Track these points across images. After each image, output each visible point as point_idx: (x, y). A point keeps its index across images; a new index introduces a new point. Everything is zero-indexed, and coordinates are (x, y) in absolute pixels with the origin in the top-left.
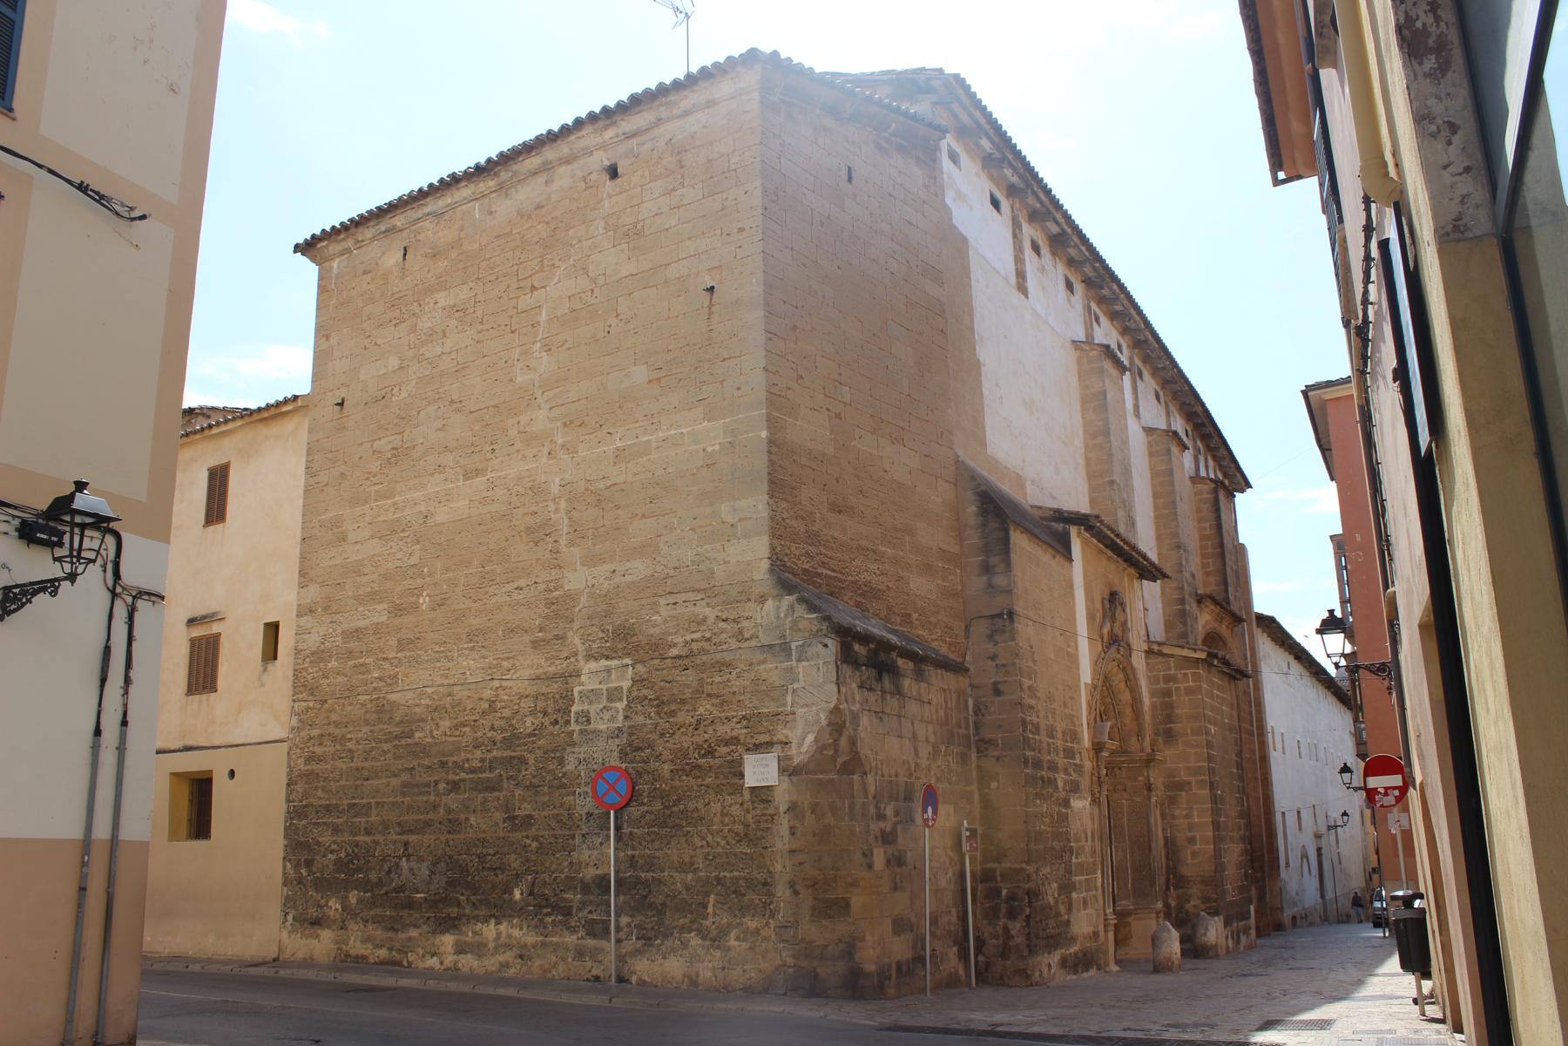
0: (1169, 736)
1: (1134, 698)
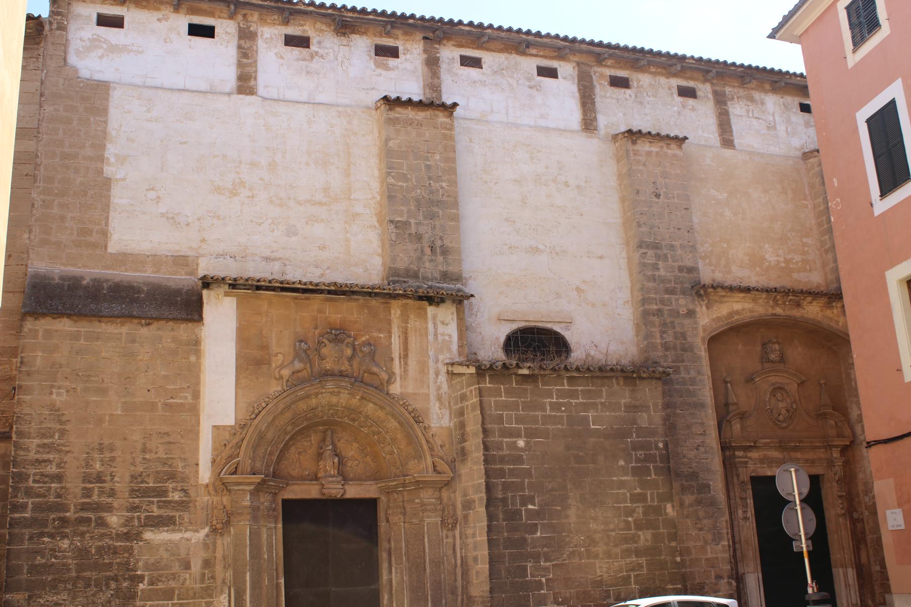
1: (400, 423)
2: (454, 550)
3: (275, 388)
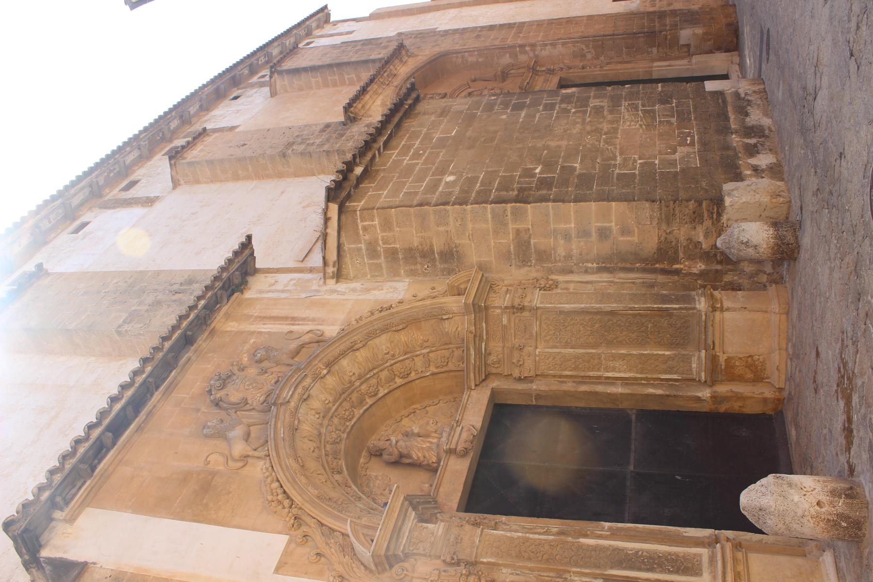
0: (450, 257)
1: (385, 330)
2: (587, 282)
3: (258, 469)
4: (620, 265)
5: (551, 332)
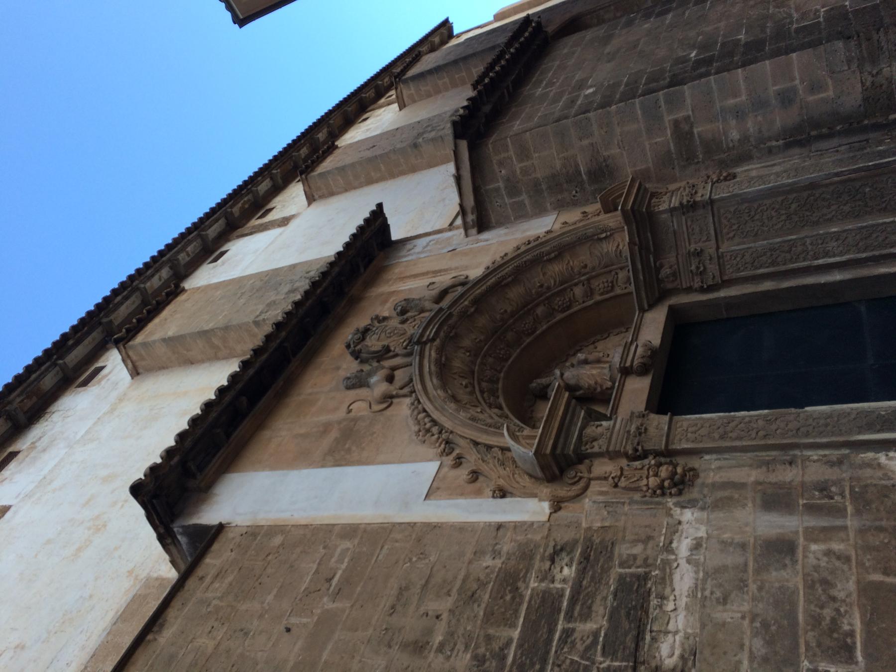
4: (814, 133)
5: (735, 227)
